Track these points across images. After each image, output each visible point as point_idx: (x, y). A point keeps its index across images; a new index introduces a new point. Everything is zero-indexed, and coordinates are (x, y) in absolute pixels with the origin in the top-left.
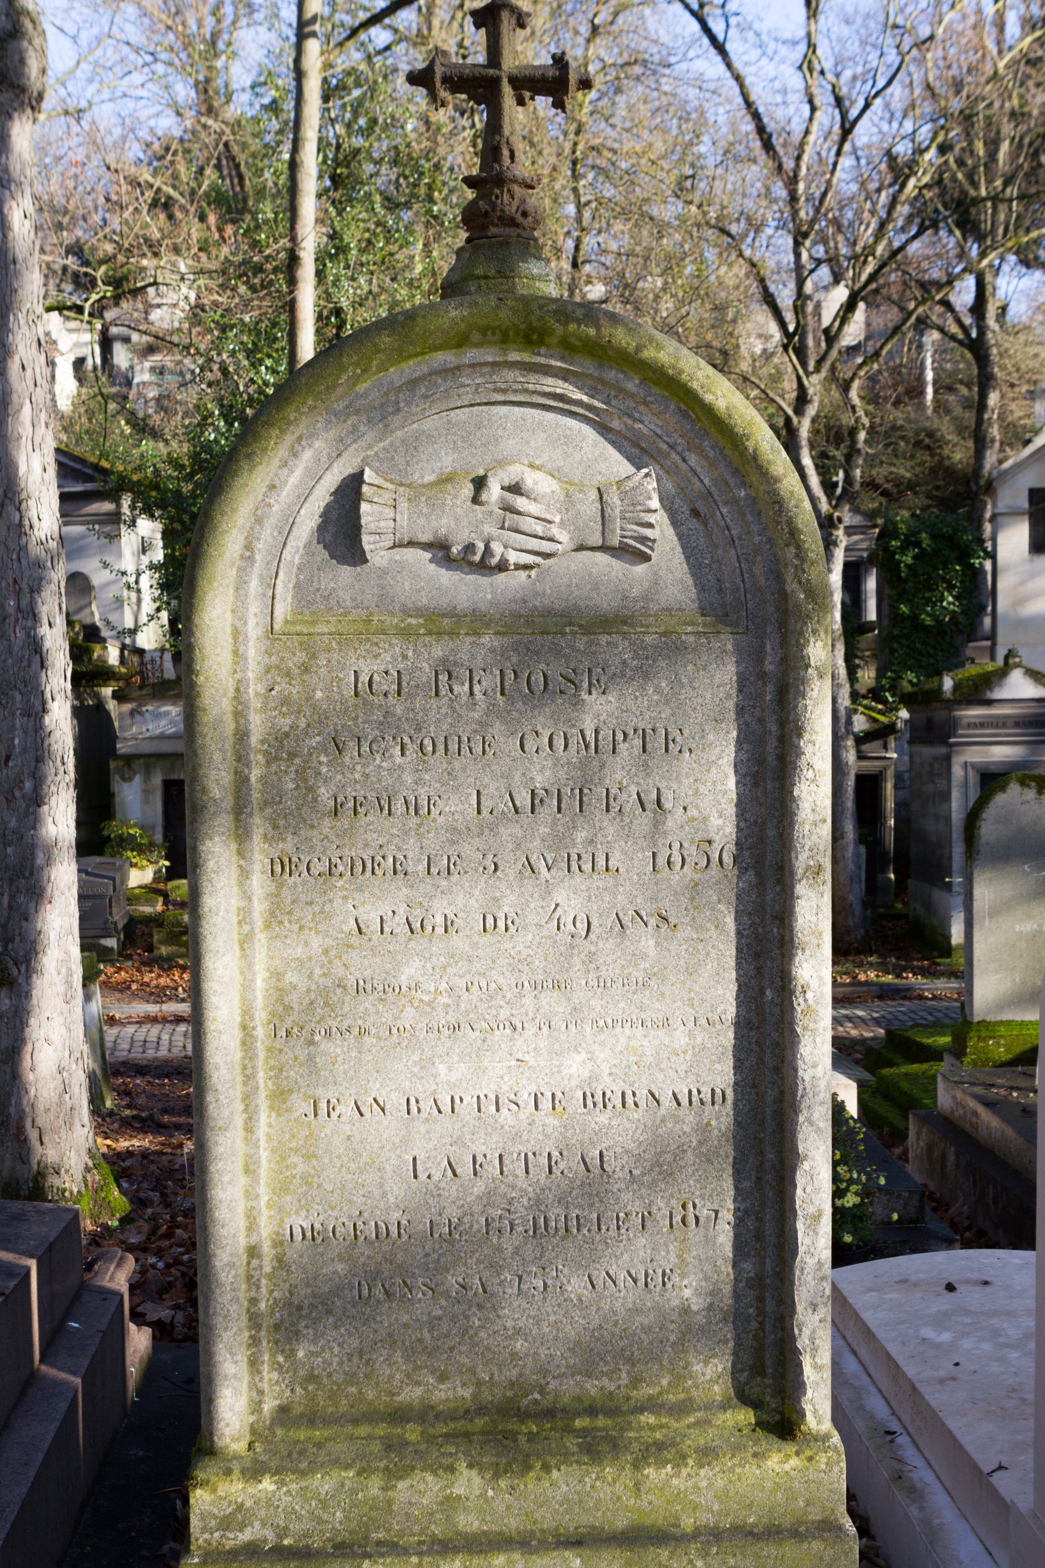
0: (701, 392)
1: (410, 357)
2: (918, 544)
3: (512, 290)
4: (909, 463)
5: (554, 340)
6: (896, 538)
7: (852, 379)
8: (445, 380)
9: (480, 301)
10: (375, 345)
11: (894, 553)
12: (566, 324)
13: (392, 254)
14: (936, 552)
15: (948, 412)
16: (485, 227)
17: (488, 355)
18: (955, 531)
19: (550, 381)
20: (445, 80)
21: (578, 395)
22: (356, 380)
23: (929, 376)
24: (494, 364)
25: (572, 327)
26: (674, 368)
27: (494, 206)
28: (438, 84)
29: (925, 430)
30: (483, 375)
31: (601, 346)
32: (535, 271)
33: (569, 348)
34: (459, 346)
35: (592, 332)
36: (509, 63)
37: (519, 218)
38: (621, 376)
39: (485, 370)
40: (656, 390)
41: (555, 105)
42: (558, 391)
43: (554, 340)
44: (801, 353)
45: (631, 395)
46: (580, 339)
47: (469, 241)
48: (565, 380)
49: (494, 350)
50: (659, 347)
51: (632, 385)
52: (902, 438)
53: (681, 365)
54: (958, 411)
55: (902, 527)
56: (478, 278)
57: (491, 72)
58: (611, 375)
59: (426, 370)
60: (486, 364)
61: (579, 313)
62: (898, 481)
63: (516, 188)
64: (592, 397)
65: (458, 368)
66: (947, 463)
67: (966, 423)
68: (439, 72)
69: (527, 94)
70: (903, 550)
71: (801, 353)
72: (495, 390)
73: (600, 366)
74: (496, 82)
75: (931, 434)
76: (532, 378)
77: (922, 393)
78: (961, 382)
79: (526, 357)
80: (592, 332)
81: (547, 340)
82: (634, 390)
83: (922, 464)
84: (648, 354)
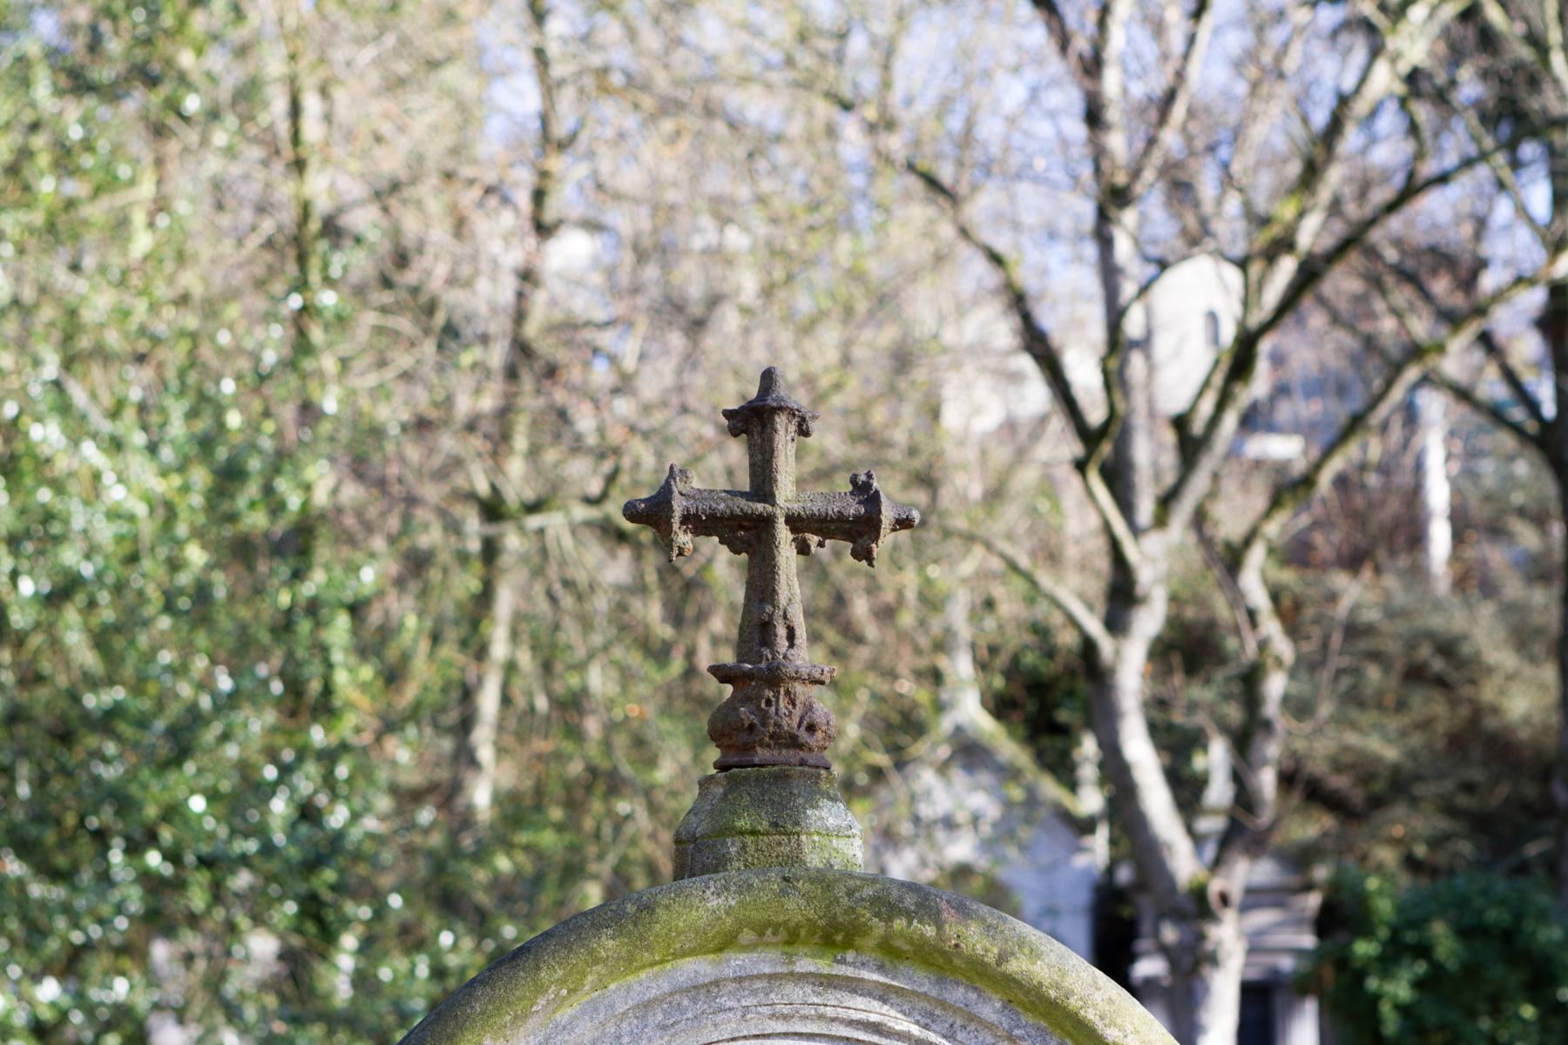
0: (1099, 1026)
1: (644, 967)
2: (1423, 951)
3: (795, 858)
4: (1394, 724)
5: (870, 942)
6: (1366, 931)
7: (1248, 541)
8: (694, 1001)
9: (756, 881)
10: (591, 952)
11: (1360, 976)
12: (890, 919)
13: (70, 204)
14: (1471, 971)
15: (1489, 589)
16: (748, 748)
17: (765, 962)
18: (1519, 917)
19: (859, 1002)
20: (686, 519)
21: (903, 1025)
22: (559, 1002)
23: (1438, 495)
24: (772, 977)
25: (899, 924)
26: (1058, 987)
27: (764, 718)
28: (676, 526)
29: (1429, 635)
30: (754, 993)
31: (944, 953)
32: (831, 822)
33: (891, 954)
34: (719, 949)
35: (930, 931)
36: (787, 494)
37: (803, 735)
38: (973, 996)
39: (758, 985)
40: (1028, 1018)
41: (856, 555)
42: (873, 1018)
43: (870, 942)
44: (1118, 478)
45: (989, 1026)
46: (911, 941)
47: (722, 767)
48: (884, 1000)
49: (774, 954)
50: (1035, 954)
51: (990, 1010)
52: (1375, 656)
53: (1068, 982)
54: (1513, 588)
55: (1384, 907)
56: (742, 833)
57: (760, 507)
58: (957, 995)
59: (666, 987)
60: (759, 977)
61: (910, 901)
62: (1364, 769)
63: (798, 688)
64: (926, 1027)
65: (716, 983)
66: (1490, 723)
67: (1538, 619)
68: (678, 506)
69: (813, 539)
70: (1387, 963)
71: (1118, 478)
72: (773, 1016)
73: (940, 981)
74: (767, 522)
75: (1447, 648)
76: (832, 997)
77: (1417, 538)
78: (1522, 512)
79: (823, 966)
80: (930, 931)
81: (858, 941)
82: (993, 1018)
83: (1425, 725)
84: (1015, 966)
